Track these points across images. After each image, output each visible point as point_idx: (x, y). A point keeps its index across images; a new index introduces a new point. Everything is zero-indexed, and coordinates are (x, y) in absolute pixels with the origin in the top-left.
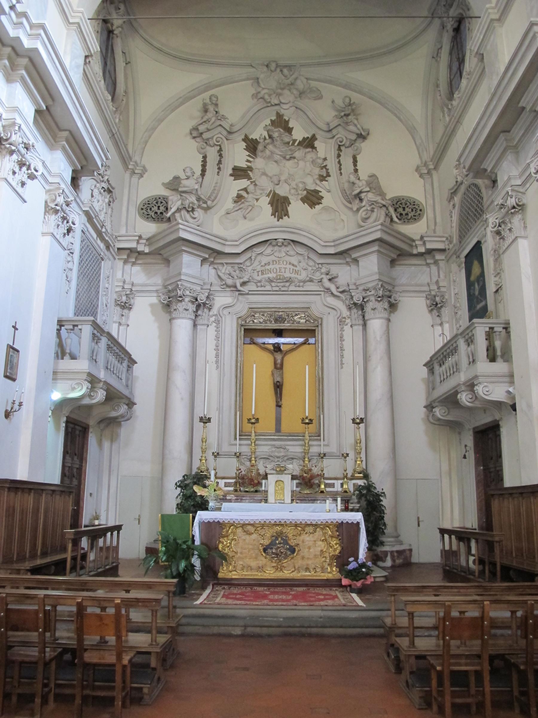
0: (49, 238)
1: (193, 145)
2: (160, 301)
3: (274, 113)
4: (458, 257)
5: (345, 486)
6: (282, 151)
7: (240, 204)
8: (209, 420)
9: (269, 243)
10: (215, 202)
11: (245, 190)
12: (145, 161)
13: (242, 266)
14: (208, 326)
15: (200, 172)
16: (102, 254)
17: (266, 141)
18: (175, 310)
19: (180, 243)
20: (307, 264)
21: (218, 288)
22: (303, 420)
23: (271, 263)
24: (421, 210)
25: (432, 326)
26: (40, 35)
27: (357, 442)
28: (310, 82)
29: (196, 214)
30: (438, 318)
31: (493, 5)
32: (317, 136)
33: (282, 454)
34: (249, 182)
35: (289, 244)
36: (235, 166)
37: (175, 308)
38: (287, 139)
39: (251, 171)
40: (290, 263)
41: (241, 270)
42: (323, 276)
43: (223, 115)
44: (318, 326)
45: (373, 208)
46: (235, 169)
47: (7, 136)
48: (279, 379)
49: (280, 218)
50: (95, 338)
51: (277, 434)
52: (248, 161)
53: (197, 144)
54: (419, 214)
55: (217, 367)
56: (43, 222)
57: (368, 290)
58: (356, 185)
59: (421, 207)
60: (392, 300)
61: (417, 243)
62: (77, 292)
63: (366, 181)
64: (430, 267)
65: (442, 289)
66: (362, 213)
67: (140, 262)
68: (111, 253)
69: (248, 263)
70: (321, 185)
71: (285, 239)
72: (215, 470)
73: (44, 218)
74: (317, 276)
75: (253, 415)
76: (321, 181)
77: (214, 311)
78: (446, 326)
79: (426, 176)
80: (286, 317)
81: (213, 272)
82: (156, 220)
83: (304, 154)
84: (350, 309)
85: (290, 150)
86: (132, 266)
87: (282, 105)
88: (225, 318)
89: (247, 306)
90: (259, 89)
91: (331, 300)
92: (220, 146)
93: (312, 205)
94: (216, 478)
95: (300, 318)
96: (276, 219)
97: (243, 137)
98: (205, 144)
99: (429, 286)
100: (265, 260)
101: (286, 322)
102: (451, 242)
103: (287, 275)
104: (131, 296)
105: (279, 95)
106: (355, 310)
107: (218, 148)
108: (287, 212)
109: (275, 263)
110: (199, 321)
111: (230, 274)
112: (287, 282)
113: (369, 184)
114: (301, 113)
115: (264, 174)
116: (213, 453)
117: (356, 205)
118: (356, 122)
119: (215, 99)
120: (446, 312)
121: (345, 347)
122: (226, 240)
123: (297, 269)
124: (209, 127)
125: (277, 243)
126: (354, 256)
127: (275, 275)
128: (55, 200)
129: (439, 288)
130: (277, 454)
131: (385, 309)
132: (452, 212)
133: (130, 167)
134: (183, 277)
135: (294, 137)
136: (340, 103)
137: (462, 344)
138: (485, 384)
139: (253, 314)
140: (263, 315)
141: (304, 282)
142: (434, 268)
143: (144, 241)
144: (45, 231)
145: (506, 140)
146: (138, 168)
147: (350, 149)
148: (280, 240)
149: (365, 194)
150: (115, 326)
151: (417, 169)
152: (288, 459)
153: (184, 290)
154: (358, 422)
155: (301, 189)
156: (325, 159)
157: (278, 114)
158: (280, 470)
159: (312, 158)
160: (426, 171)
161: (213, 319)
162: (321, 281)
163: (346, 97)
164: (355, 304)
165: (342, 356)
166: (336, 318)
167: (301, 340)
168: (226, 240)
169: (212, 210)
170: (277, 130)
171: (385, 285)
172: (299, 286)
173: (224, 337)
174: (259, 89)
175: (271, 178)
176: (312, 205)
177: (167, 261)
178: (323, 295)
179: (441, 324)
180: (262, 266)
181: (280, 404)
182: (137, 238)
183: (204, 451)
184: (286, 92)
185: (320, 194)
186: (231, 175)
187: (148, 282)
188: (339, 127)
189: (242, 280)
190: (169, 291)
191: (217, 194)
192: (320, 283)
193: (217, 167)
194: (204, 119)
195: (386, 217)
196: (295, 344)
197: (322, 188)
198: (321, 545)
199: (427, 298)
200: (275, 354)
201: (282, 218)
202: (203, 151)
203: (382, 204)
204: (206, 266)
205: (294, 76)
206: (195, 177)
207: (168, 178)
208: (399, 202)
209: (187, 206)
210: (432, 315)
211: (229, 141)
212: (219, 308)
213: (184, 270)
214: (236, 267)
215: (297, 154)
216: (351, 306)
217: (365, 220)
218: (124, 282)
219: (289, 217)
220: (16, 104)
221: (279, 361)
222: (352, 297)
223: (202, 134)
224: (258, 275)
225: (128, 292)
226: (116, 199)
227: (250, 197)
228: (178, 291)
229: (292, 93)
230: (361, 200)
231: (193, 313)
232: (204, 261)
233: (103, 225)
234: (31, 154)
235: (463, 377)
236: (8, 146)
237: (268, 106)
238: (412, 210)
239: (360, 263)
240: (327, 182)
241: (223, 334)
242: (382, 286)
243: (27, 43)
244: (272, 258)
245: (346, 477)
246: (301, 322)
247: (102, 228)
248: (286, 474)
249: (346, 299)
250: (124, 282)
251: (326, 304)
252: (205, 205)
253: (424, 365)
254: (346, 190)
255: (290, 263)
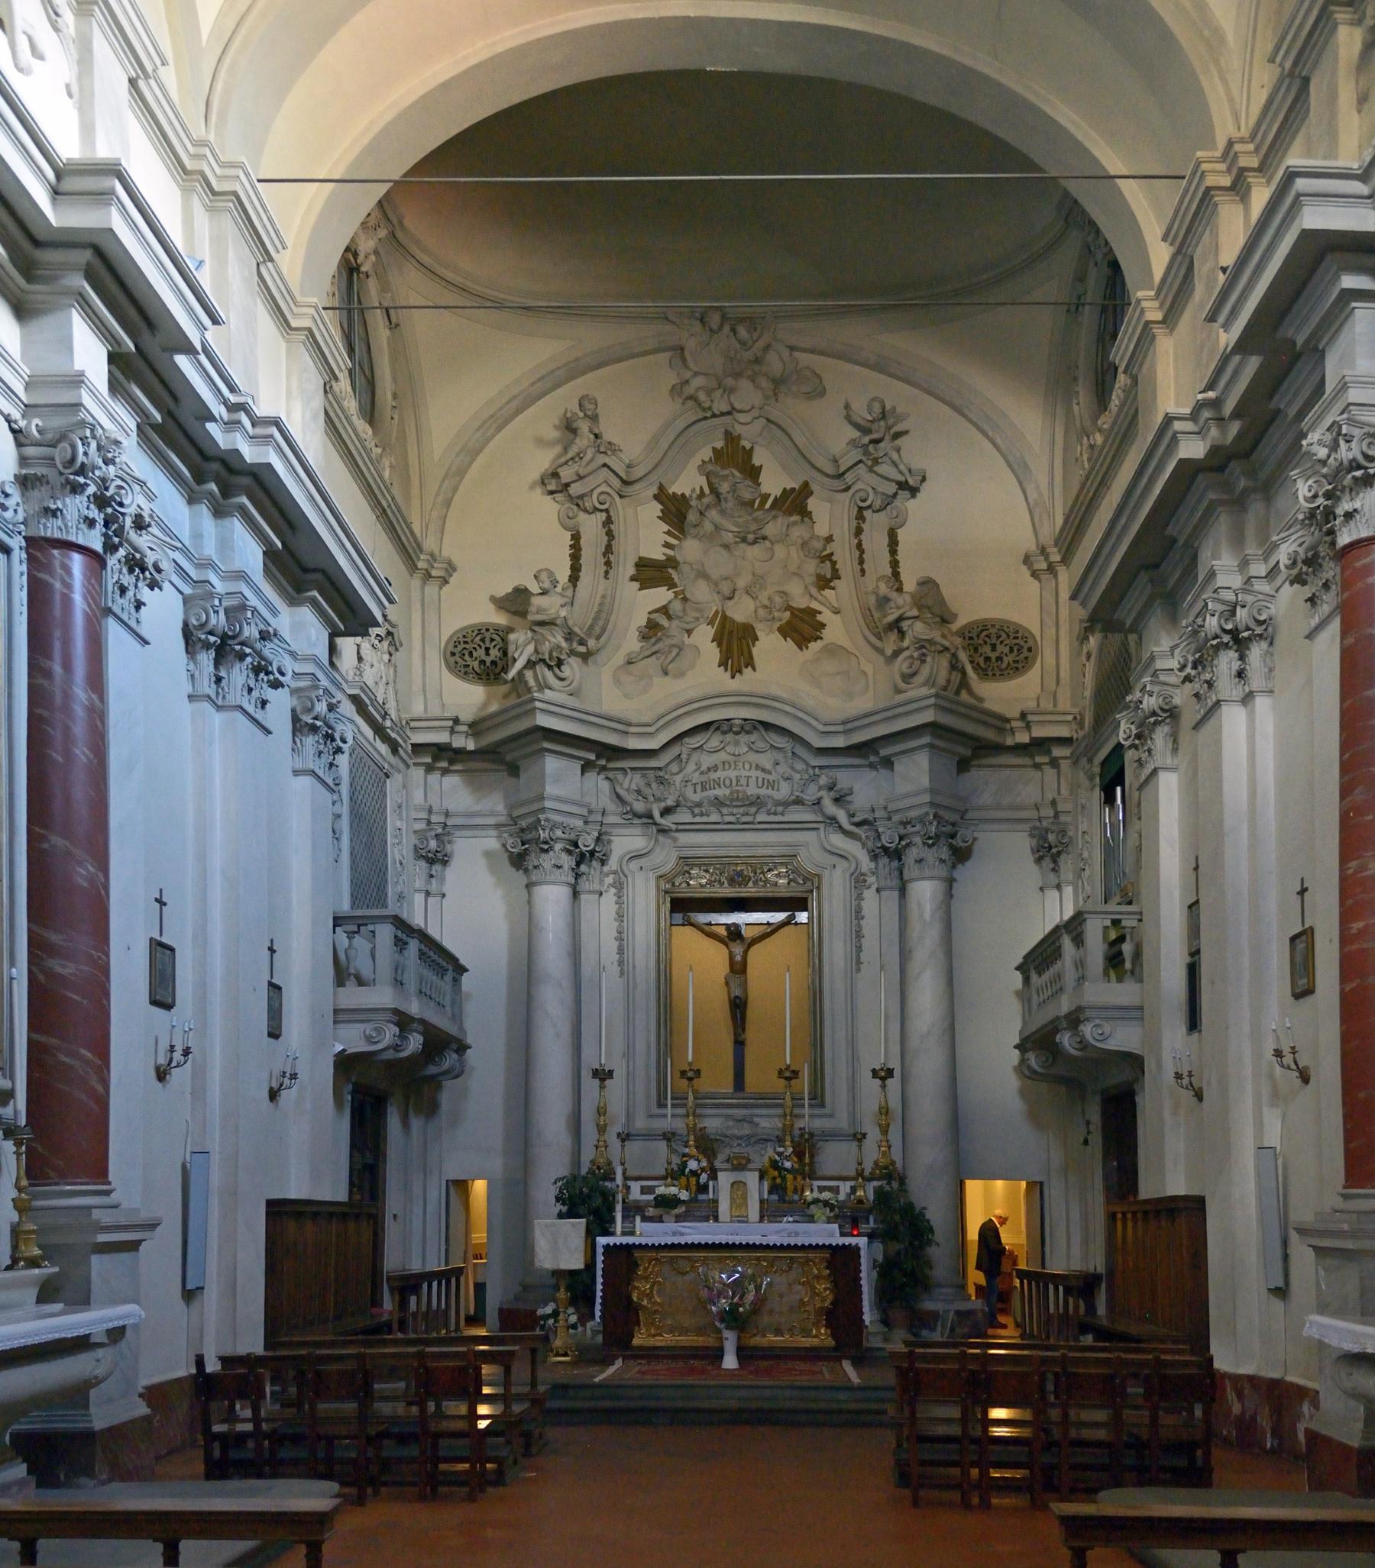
0: (307, 781)
1: (548, 509)
2: (504, 845)
3: (720, 434)
4: (1090, 760)
5: (860, 1193)
6: (737, 525)
7: (654, 644)
8: (610, 1074)
9: (712, 728)
10: (603, 640)
11: (664, 610)
12: (449, 551)
13: (661, 774)
14: (601, 894)
15: (569, 573)
16: (386, 766)
17: (706, 500)
18: (535, 867)
19: (539, 735)
20: (792, 768)
21: (618, 820)
22: (780, 1072)
23: (720, 767)
24: (1030, 650)
25: (1041, 889)
26: (272, 436)
27: (885, 1111)
28: (796, 354)
29: (566, 671)
30: (1052, 875)
31: (1218, 154)
32: (814, 487)
33: (747, 1132)
34: (670, 594)
35: (755, 728)
36: (640, 558)
37: (536, 863)
38: (747, 495)
39: (675, 568)
40: (757, 767)
41: (661, 781)
42: (823, 793)
43: (609, 443)
44: (812, 891)
45: (924, 655)
46: (642, 564)
47: (234, 631)
48: (738, 992)
49: (736, 671)
50: (400, 944)
51: (739, 1095)
52: (667, 545)
53: (557, 507)
54: (1026, 658)
55: (622, 973)
56: (293, 750)
57: (909, 823)
58: (892, 604)
59: (1030, 643)
60: (958, 842)
61: (1014, 724)
62: (351, 854)
63: (913, 595)
64: (1041, 770)
65: (1063, 818)
66: (902, 663)
67: (458, 767)
68: (401, 758)
69: (674, 768)
70: (820, 598)
71: (745, 720)
72: (622, 1164)
73: (294, 742)
74: (811, 793)
75: (690, 1064)
76: (821, 588)
77: (613, 864)
78: (1068, 891)
79: (1044, 577)
80: (752, 875)
81: (605, 786)
82: (484, 677)
83: (785, 528)
84: (875, 857)
85: (755, 520)
86: (442, 775)
87: (736, 414)
88: (633, 879)
89: (674, 856)
90: (688, 375)
91: (838, 841)
92: (607, 511)
93: (802, 642)
94: (626, 1178)
95: (778, 875)
96: (729, 673)
97: (654, 490)
98: (575, 508)
99: (1038, 810)
100: (707, 761)
101: (750, 884)
102: (1081, 725)
103: (752, 791)
104: (446, 838)
105: (731, 390)
106: (886, 860)
107: (604, 515)
108: (751, 657)
109: (727, 766)
110: (584, 885)
111: (639, 792)
112: (751, 804)
113: (918, 602)
114: (779, 433)
115: (703, 575)
116: (619, 1135)
117: (890, 644)
118: (895, 456)
119: (592, 407)
120: (1067, 864)
121: (865, 931)
122: (630, 725)
123: (771, 778)
124: (582, 472)
125: (731, 726)
126: (884, 752)
127: (727, 792)
128: (310, 710)
129: (1057, 814)
130: (736, 1132)
131: (942, 861)
132: (1084, 665)
133: (420, 565)
134: (548, 804)
135: (765, 488)
136: (861, 412)
137: (1067, 943)
138: (1097, 1021)
139: (686, 868)
140: (707, 871)
141: (786, 804)
142: (1050, 772)
143: (465, 728)
144: (299, 766)
145: (1152, 581)
146: (436, 565)
147: (882, 514)
148: (737, 722)
149: (909, 622)
150: (419, 898)
151: (1027, 560)
152: (755, 1142)
153: (551, 829)
154: (883, 1075)
155: (777, 607)
156: (829, 539)
157: (728, 434)
158: (740, 1164)
159: (801, 537)
160: (1044, 566)
161: (610, 880)
162: (818, 802)
163: (874, 399)
164: (885, 849)
165: (859, 949)
166: (848, 874)
167: (779, 917)
168: (630, 725)
169: (600, 658)
170: (726, 472)
171: (941, 812)
172: (775, 814)
173: (634, 914)
174: (688, 375)
175: (716, 584)
176: (802, 642)
177: (514, 770)
178: (822, 832)
179: (1058, 887)
180: (702, 773)
181: (740, 1039)
182: (450, 723)
183: (602, 1129)
184: (745, 384)
185: (819, 617)
186: (633, 579)
187: (477, 808)
188: (861, 465)
189: (663, 805)
190: (522, 830)
191: (607, 621)
192: (816, 807)
193: (603, 560)
194: (570, 455)
195: (950, 674)
196: (768, 924)
197: (824, 604)
198: (801, 1293)
199: (1032, 836)
200: (731, 944)
201: (740, 672)
202: (570, 523)
203: (942, 645)
204: (591, 775)
205: (761, 344)
206: (559, 589)
207: (505, 589)
208: (985, 633)
209: (547, 657)
210: (1041, 868)
211: (625, 500)
212: (621, 859)
213: (550, 789)
214: (651, 774)
215: (770, 529)
216: (877, 851)
217: (907, 678)
218: (430, 811)
219: (754, 669)
220: (237, 565)
221: (738, 958)
222: (879, 836)
223: (567, 485)
224: (695, 792)
225: (440, 831)
226: (401, 645)
227: (673, 628)
228: (541, 832)
229: (757, 387)
230: (902, 634)
231: (570, 872)
232: (586, 767)
233: (386, 713)
234: (272, 645)
235: (1065, 1006)
236: (238, 648)
237: (705, 418)
238: (1011, 650)
239: (896, 767)
240: (833, 592)
241: (630, 910)
242: (935, 816)
243: (250, 454)
244: (723, 756)
245: (860, 1174)
246: (779, 882)
247: (384, 718)
248: (751, 1170)
249: (867, 837)
250: (430, 811)
251: (829, 848)
252: (582, 649)
253: (1017, 969)
254: (873, 609)
255: (757, 767)
